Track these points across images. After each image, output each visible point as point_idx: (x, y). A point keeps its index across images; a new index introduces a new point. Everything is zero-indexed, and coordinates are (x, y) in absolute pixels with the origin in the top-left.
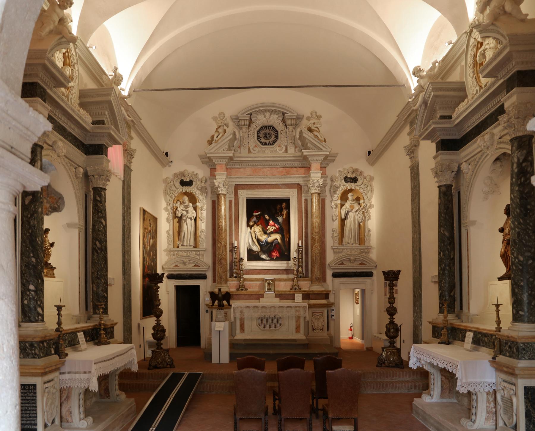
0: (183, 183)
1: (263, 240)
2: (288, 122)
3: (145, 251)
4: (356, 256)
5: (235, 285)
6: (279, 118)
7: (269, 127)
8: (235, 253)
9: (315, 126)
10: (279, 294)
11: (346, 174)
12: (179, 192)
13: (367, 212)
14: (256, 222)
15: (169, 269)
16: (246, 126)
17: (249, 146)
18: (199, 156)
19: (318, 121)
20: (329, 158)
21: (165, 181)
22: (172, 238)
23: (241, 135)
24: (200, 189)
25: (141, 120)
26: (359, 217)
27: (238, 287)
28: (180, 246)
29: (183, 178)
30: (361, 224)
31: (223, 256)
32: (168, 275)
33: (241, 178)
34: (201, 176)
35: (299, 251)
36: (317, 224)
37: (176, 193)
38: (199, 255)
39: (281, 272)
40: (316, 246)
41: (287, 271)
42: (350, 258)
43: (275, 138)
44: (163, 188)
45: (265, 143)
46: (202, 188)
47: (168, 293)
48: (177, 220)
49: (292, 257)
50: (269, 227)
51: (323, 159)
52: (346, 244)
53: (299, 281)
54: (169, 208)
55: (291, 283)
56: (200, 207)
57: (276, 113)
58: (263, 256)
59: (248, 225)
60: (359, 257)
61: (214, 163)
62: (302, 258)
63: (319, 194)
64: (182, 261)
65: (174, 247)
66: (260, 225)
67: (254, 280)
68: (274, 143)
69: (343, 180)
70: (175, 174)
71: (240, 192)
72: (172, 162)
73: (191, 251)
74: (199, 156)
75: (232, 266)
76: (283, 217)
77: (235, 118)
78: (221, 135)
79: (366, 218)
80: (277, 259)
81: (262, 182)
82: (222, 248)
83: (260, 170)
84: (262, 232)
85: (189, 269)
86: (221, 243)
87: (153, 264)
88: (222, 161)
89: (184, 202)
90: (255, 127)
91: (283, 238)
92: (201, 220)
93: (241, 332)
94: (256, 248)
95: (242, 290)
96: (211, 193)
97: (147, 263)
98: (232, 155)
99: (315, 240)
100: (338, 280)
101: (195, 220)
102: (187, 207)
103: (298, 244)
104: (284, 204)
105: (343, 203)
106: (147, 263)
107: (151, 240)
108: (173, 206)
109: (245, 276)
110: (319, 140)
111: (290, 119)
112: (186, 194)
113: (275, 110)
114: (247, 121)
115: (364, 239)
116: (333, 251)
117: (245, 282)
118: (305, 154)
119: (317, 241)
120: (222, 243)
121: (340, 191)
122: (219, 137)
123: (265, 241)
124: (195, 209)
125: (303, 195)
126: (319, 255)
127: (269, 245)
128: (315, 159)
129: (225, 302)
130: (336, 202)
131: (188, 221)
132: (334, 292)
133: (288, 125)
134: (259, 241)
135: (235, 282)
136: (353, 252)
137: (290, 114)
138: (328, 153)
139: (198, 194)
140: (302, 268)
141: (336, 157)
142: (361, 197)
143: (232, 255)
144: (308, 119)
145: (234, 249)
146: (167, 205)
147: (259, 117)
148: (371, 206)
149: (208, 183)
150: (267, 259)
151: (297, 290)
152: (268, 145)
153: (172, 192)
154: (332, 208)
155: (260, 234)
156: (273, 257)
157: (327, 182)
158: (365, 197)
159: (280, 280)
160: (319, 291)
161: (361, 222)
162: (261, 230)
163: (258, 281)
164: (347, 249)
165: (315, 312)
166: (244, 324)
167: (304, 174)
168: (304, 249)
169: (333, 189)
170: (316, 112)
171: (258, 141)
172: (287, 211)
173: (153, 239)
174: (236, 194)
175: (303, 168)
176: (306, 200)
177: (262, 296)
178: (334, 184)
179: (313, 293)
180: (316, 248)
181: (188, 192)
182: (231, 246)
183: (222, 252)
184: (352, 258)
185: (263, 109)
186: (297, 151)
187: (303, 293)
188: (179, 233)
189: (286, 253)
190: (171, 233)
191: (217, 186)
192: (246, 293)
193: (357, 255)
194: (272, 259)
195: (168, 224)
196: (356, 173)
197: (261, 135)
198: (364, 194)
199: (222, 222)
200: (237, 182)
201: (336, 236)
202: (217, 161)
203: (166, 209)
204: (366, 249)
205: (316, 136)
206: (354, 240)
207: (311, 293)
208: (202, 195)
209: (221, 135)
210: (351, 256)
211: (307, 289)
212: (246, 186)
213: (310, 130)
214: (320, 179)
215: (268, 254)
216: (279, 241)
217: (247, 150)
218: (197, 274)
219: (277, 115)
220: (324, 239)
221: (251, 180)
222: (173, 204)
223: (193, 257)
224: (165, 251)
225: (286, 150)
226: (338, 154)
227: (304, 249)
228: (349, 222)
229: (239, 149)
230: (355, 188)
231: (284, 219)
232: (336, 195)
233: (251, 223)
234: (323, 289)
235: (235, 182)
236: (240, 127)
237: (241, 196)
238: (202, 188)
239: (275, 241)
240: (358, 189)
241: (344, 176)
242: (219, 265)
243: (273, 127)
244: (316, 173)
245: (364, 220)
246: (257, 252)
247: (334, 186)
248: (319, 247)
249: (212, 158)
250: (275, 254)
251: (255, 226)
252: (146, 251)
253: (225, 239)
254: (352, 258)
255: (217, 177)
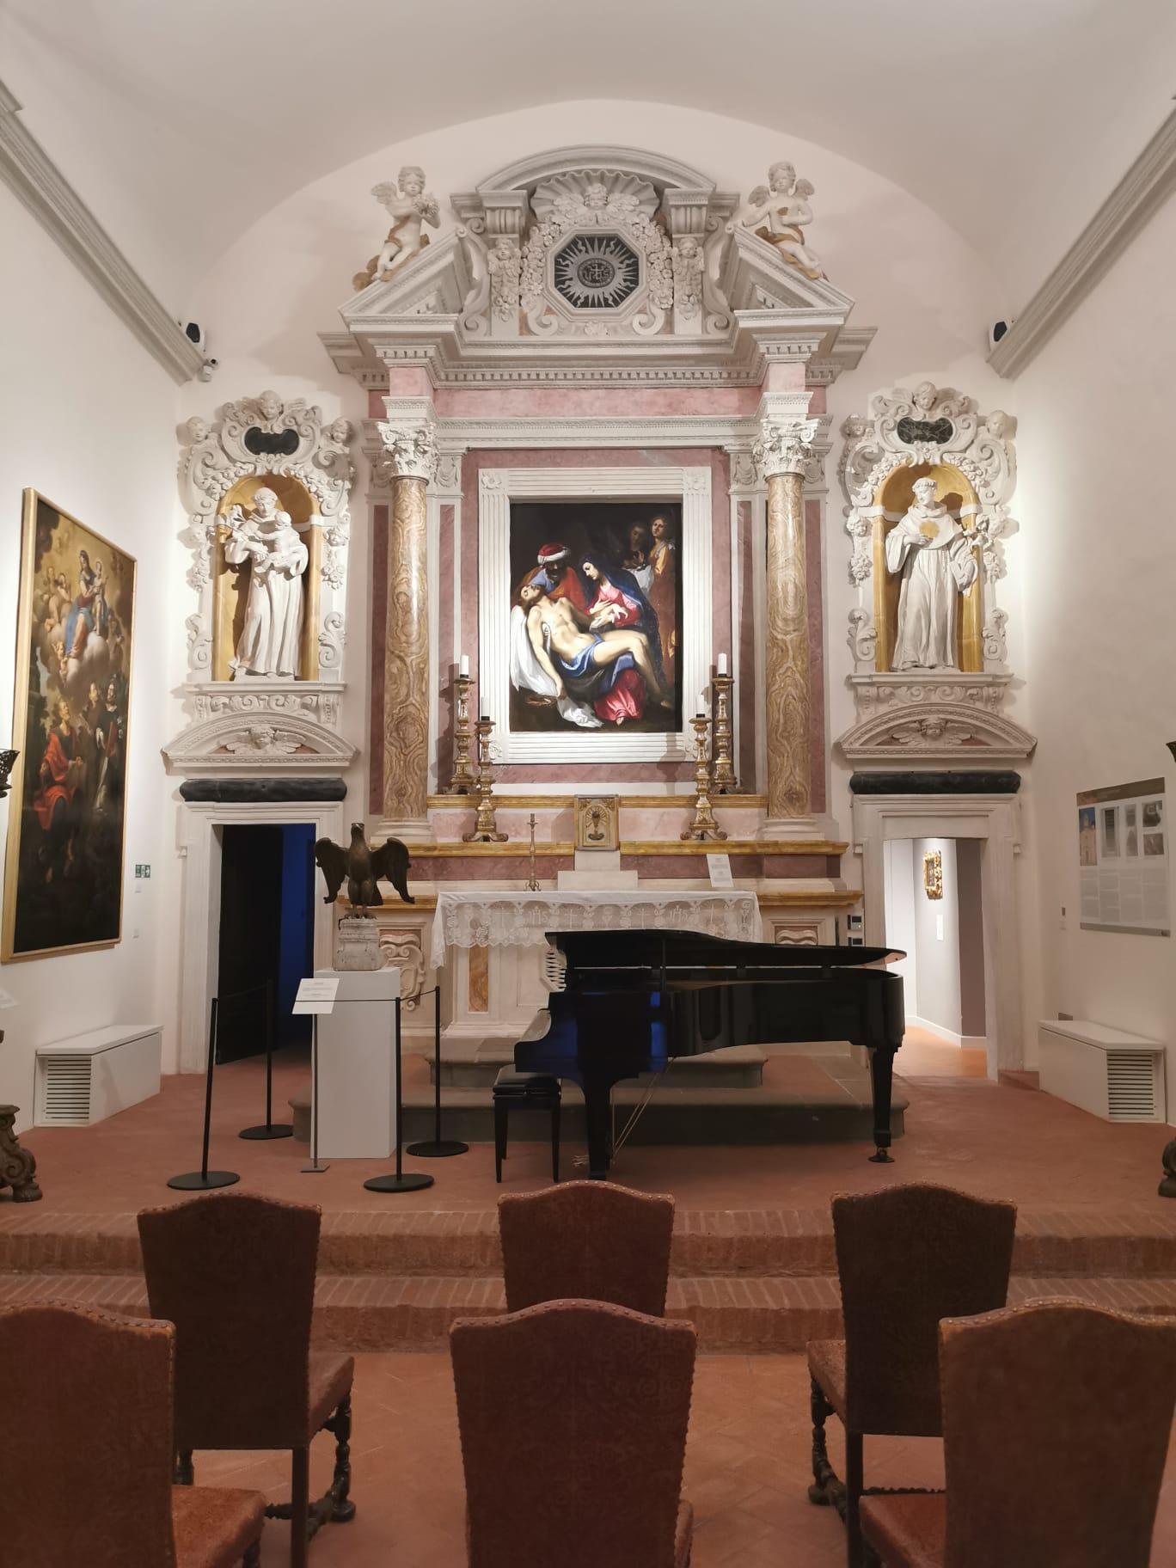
0: (258, 442)
1: (573, 656)
2: (677, 219)
3: (45, 676)
4: (951, 713)
5: (458, 823)
6: (642, 208)
7: (601, 240)
8: (463, 702)
9: (786, 219)
10: (637, 856)
11: (907, 408)
12: (242, 473)
13: (989, 549)
14: (548, 587)
15: (190, 760)
16: (514, 232)
17: (521, 312)
18: (323, 337)
19: (800, 202)
20: (837, 348)
21: (185, 433)
22: (209, 645)
23: (493, 268)
24: (326, 463)
25: (19, 107)
26: (960, 566)
27: (470, 830)
28: (240, 674)
29: (258, 423)
30: (966, 592)
31: (411, 709)
32: (185, 784)
33: (488, 424)
34: (328, 419)
35: (715, 694)
36: (791, 588)
37: (228, 478)
38: (316, 709)
39: (644, 774)
40: (789, 674)
41: (669, 769)
42: (923, 720)
43: (625, 280)
44: (179, 459)
45: (587, 298)
46: (334, 460)
47: (184, 852)
48: (231, 577)
49: (688, 713)
50: (598, 606)
51: (815, 348)
52: (908, 665)
53: (720, 806)
54: (200, 532)
55: (684, 812)
56: (325, 530)
57: (631, 189)
58: (575, 715)
59: (516, 599)
60: (961, 714)
61: (381, 360)
62: (729, 721)
63: (799, 477)
64: (249, 730)
65: (214, 679)
66: (564, 600)
67: (535, 801)
68: (622, 299)
69: (895, 433)
70: (228, 406)
71: (486, 476)
72: (214, 361)
73: (285, 693)
74: (323, 337)
75: (451, 752)
76: (654, 567)
77: (468, 202)
78: (407, 251)
79: (986, 572)
80: (630, 725)
81: (573, 439)
82: (404, 678)
83: (565, 395)
84: (572, 626)
85: (272, 760)
86: (402, 660)
87: (100, 734)
88: (411, 353)
89: (259, 513)
90: (548, 240)
91: (653, 649)
92: (329, 579)
93: (473, 1007)
94: (547, 684)
95: (486, 839)
96: (372, 480)
97: (63, 726)
98: (450, 328)
99: (784, 651)
100: (872, 806)
101: (306, 577)
102: (270, 527)
103: (714, 669)
104: (659, 522)
105: (891, 517)
106: (63, 726)
107: (94, 640)
108: (217, 527)
109: (498, 789)
110: (802, 270)
111: (685, 206)
112: (269, 480)
113: (626, 174)
114: (518, 212)
115: (981, 651)
116: (851, 694)
117: (498, 811)
118: (743, 324)
119: (791, 653)
120: (408, 660)
121: (881, 474)
122: (400, 258)
123: (584, 657)
124: (306, 538)
125: (734, 487)
126: (798, 706)
127: (600, 673)
128: (784, 348)
129: (386, 888)
130: (864, 512)
131: (276, 579)
132: (858, 850)
133: (679, 232)
134: (556, 657)
135: (458, 811)
136: (935, 698)
137: (684, 188)
138: (839, 321)
139: (317, 482)
140: (731, 755)
141: (867, 342)
142: (967, 494)
143: (452, 711)
144: (758, 197)
145: (456, 687)
146: (192, 521)
147: (563, 202)
148: (1007, 528)
149: (361, 442)
150: (590, 724)
151: (708, 841)
152: (600, 305)
153: (210, 472)
154: (849, 534)
155: (563, 634)
156: (613, 718)
157: (829, 440)
158: (982, 492)
159: (641, 802)
160: (800, 845)
161: (969, 584)
162: (567, 616)
163: (552, 806)
164: (910, 685)
165: (784, 928)
166: (485, 974)
167: (739, 410)
168: (736, 686)
169: (853, 465)
170: (790, 169)
171: (561, 290)
172: (670, 547)
173: (104, 633)
174: (470, 483)
175: (735, 390)
176: (746, 506)
177: (567, 862)
178: (858, 447)
179: (776, 851)
180: (788, 681)
181: (280, 476)
182: (446, 677)
183: (408, 695)
184: (932, 719)
185: (579, 172)
186: (710, 327)
187: (737, 851)
188: (240, 625)
189: (663, 704)
190: (206, 626)
191: (391, 447)
192: (501, 853)
193: (950, 709)
194: (609, 726)
195: (195, 594)
196: (947, 407)
197: (571, 272)
198: (978, 480)
199: (408, 583)
200: (475, 439)
201: (865, 640)
202: (390, 353)
203: (188, 538)
204: (990, 685)
205: (793, 260)
206: (938, 654)
207: (770, 850)
208: (333, 486)
209: (407, 251)
210: (930, 712)
211: (750, 838)
212: (508, 456)
213: (767, 236)
214: (802, 420)
215: (593, 708)
216: (640, 658)
217: (514, 323)
218: (305, 782)
219: (634, 194)
220: (819, 650)
221: (528, 432)
222: (216, 519)
223: (294, 714)
224: (177, 693)
225: (669, 326)
226: (876, 330)
227: (736, 686)
228: (914, 590)
229: (483, 322)
230: (942, 458)
231: (656, 576)
232: (866, 489)
233: (529, 593)
234: (820, 837)
235: (467, 439)
236: (487, 236)
237: (490, 492)
238: (333, 463)
239: (621, 658)
240: (956, 462)
241: (898, 419)
242: (392, 745)
243: (619, 243)
244: (787, 399)
245: (978, 579)
246: (549, 697)
247: (857, 453)
248: (798, 676)
249: (371, 341)
250: (623, 706)
251: (544, 602)
252: (56, 680)
253: (421, 647)
254: (932, 719)
255: (390, 413)
